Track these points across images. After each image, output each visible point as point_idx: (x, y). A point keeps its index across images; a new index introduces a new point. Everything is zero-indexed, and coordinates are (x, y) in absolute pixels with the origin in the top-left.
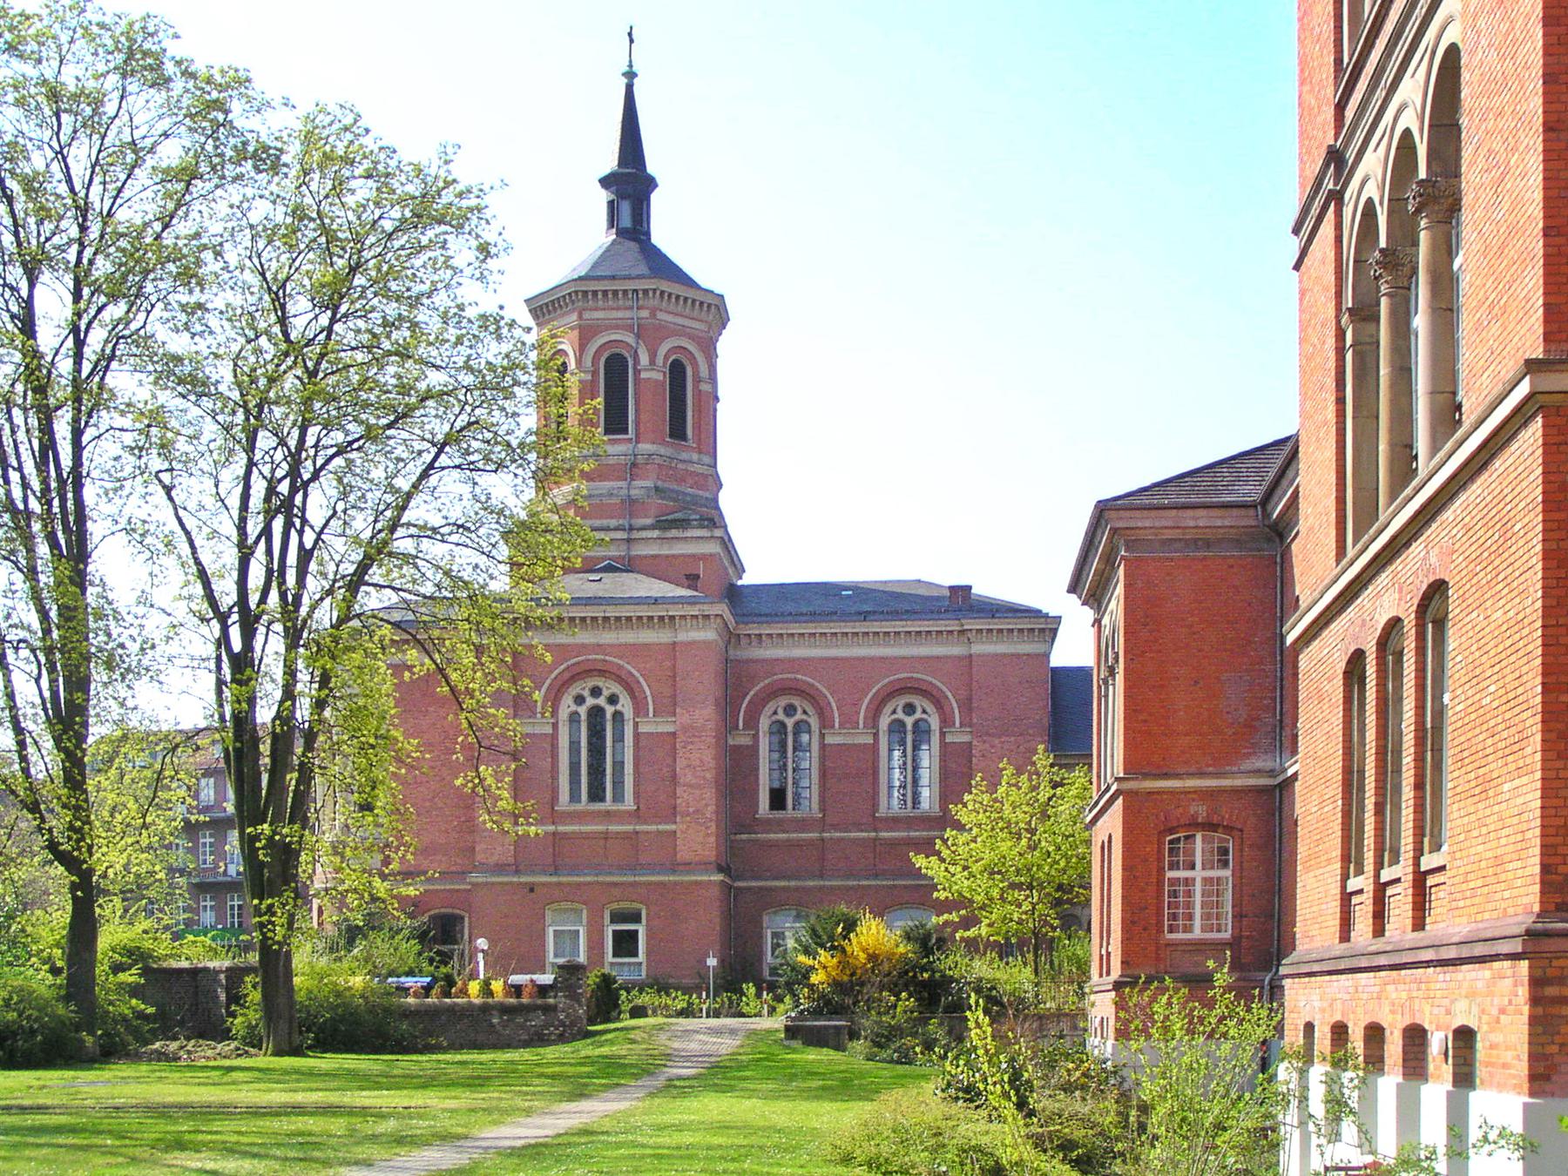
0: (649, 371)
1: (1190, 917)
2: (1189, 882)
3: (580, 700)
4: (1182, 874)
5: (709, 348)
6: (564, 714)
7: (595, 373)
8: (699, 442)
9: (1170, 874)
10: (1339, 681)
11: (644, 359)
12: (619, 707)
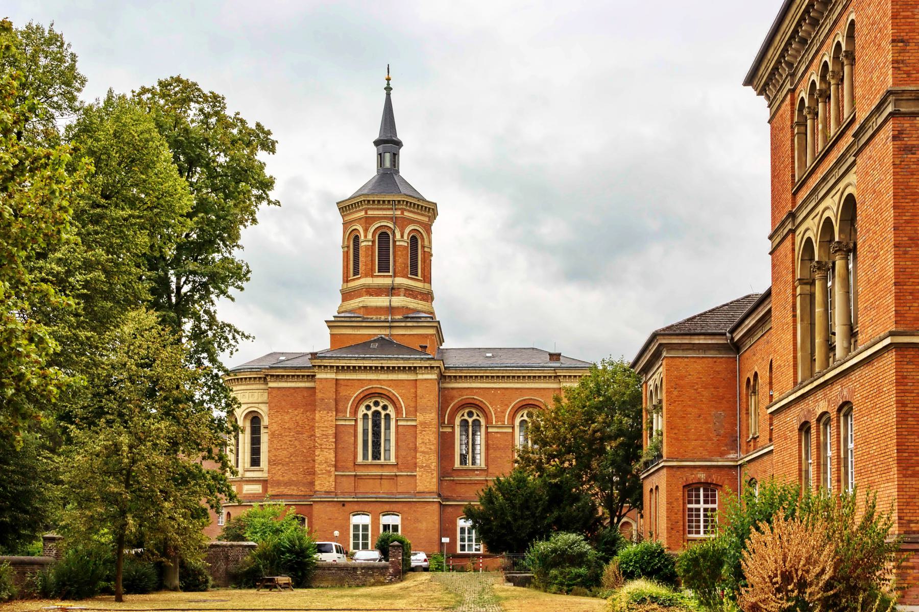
0: (401, 239)
1: (699, 527)
2: (698, 510)
3: (368, 408)
4: (694, 506)
5: (428, 228)
6: (360, 415)
7: (373, 242)
8: (424, 276)
9: (690, 506)
10: (796, 432)
11: (398, 236)
12: (388, 412)
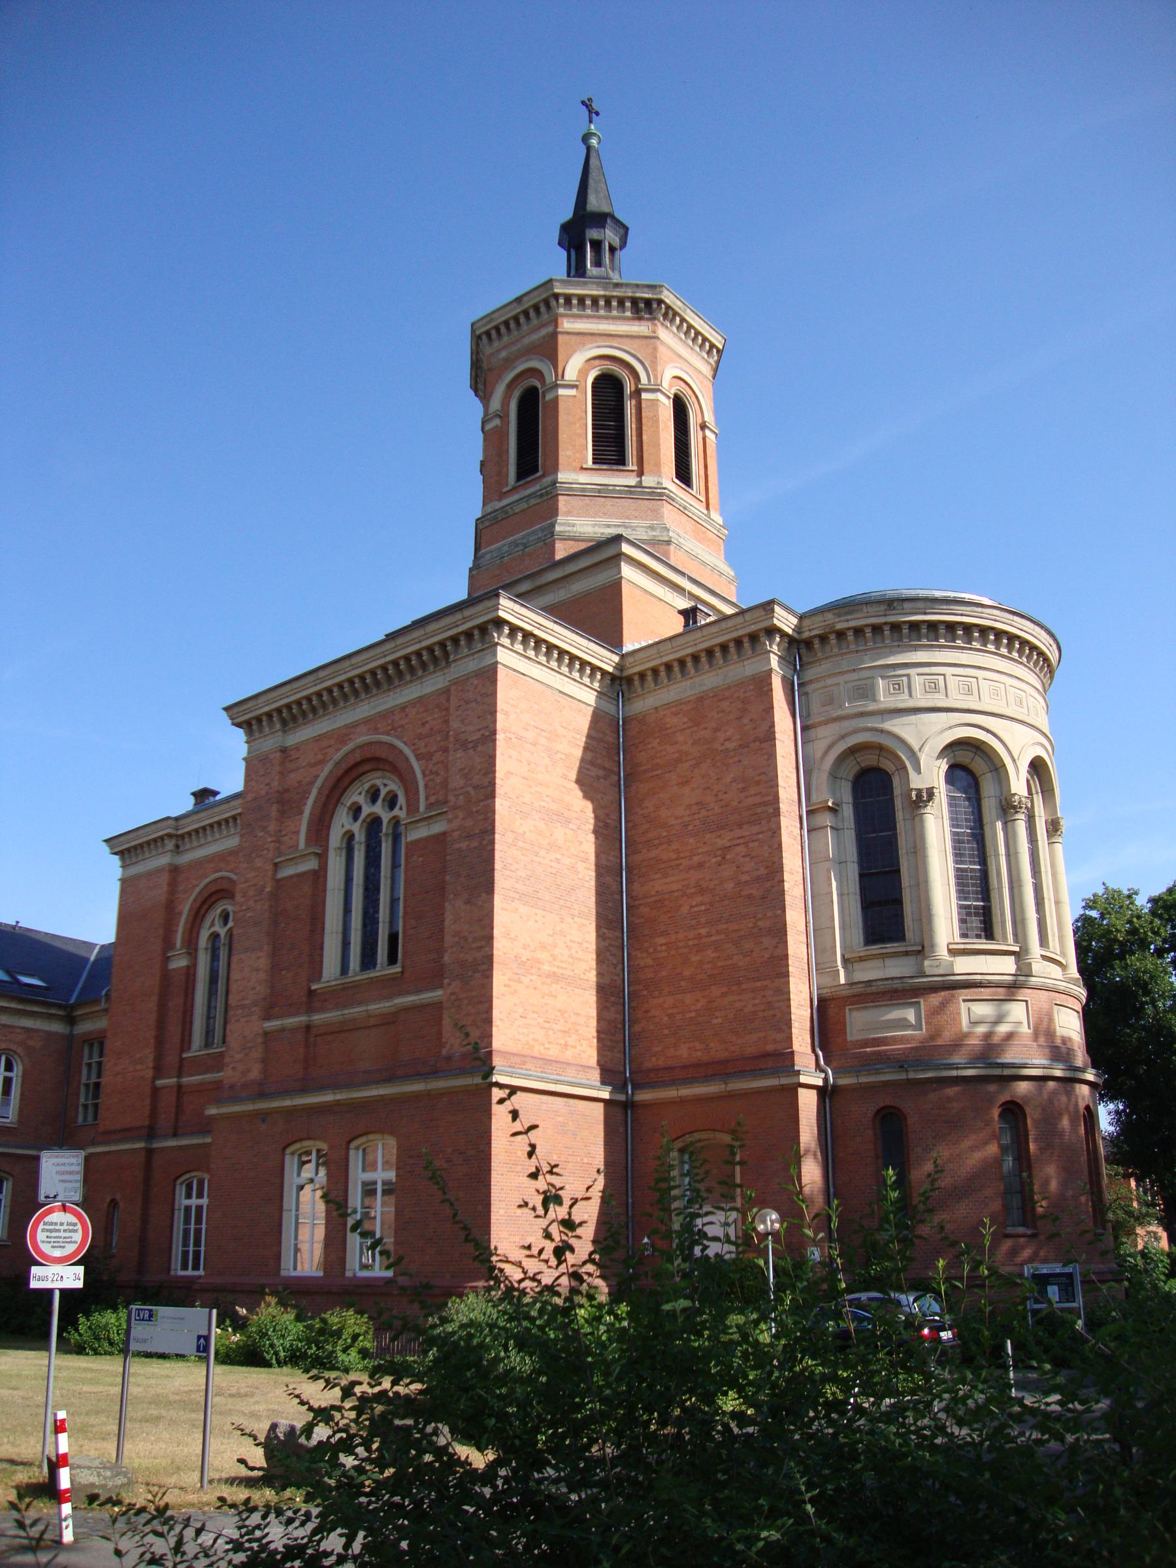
6: (335, 838)
